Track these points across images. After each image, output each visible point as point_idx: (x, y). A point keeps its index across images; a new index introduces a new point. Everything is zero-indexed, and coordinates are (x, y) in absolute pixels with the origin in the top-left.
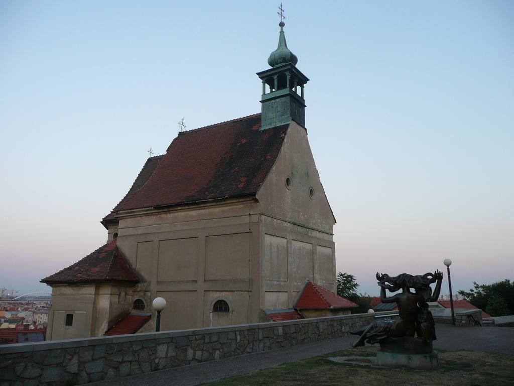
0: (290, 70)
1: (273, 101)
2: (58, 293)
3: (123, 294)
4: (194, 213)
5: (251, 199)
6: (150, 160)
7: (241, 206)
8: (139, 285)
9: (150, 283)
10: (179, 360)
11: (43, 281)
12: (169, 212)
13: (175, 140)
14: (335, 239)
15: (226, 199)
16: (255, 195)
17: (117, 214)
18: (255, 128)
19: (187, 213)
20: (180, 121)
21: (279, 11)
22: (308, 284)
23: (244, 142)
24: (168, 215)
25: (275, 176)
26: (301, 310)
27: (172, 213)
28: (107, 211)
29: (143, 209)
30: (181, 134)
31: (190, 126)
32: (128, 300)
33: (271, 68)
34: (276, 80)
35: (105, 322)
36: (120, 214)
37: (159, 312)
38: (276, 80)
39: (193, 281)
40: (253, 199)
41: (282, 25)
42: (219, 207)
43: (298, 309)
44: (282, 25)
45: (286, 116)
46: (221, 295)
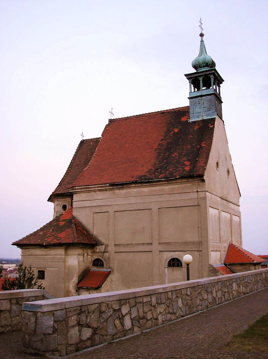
0: (214, 74)
1: (199, 98)
2: (27, 254)
3: (86, 254)
4: (146, 190)
5: (199, 179)
6: (83, 143)
7: (189, 185)
8: (98, 247)
9: (107, 246)
10: (196, 297)
11: (14, 244)
12: (122, 188)
13: (107, 126)
14: (241, 209)
15: (176, 179)
16: (203, 177)
17: (72, 190)
18: (183, 119)
19: (139, 189)
20: (110, 110)
21: (200, 24)
22: (230, 245)
23: (176, 131)
24: (121, 190)
25: (212, 161)
26: (229, 265)
27: (125, 189)
28: (52, 184)
29: (98, 186)
30: (111, 121)
31: (119, 115)
32: (89, 259)
33: (194, 71)
34: (201, 82)
35: (75, 276)
36: (75, 189)
37: (188, 265)
38: (201, 82)
39: (148, 244)
40: (201, 180)
41: (202, 35)
42: (169, 185)
43: (227, 264)
44: (202, 35)
45: (211, 111)
46: (174, 254)
